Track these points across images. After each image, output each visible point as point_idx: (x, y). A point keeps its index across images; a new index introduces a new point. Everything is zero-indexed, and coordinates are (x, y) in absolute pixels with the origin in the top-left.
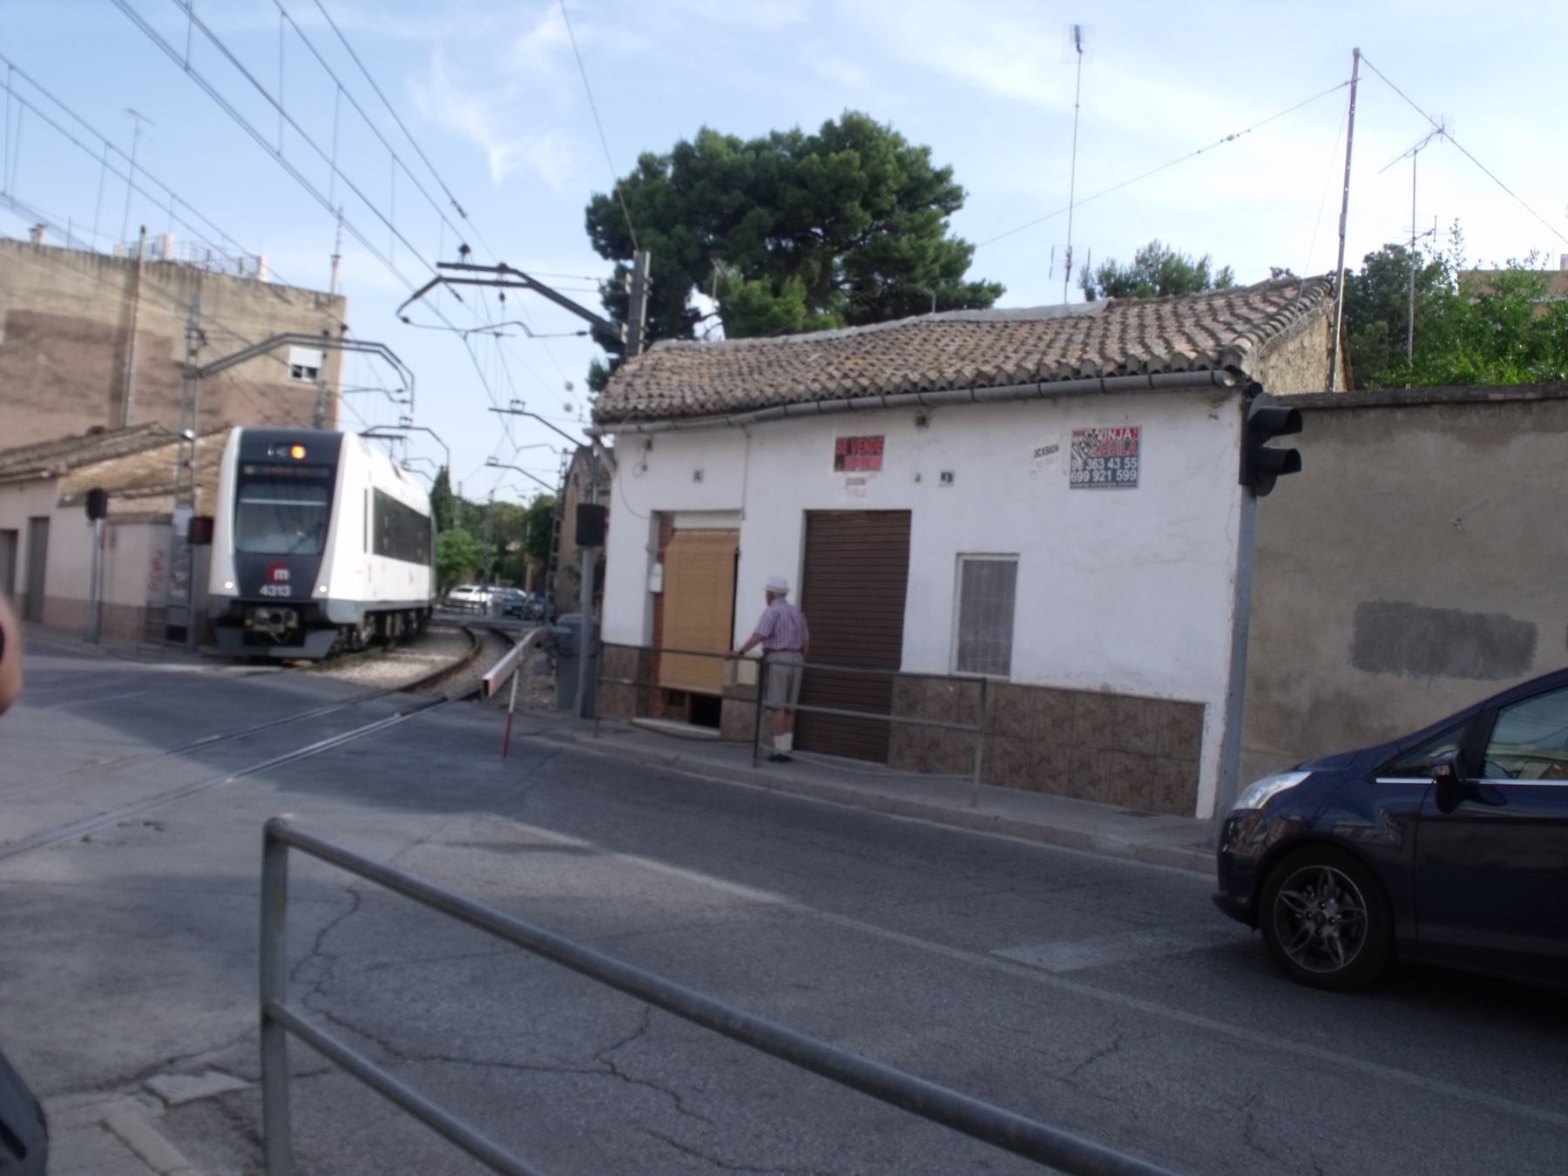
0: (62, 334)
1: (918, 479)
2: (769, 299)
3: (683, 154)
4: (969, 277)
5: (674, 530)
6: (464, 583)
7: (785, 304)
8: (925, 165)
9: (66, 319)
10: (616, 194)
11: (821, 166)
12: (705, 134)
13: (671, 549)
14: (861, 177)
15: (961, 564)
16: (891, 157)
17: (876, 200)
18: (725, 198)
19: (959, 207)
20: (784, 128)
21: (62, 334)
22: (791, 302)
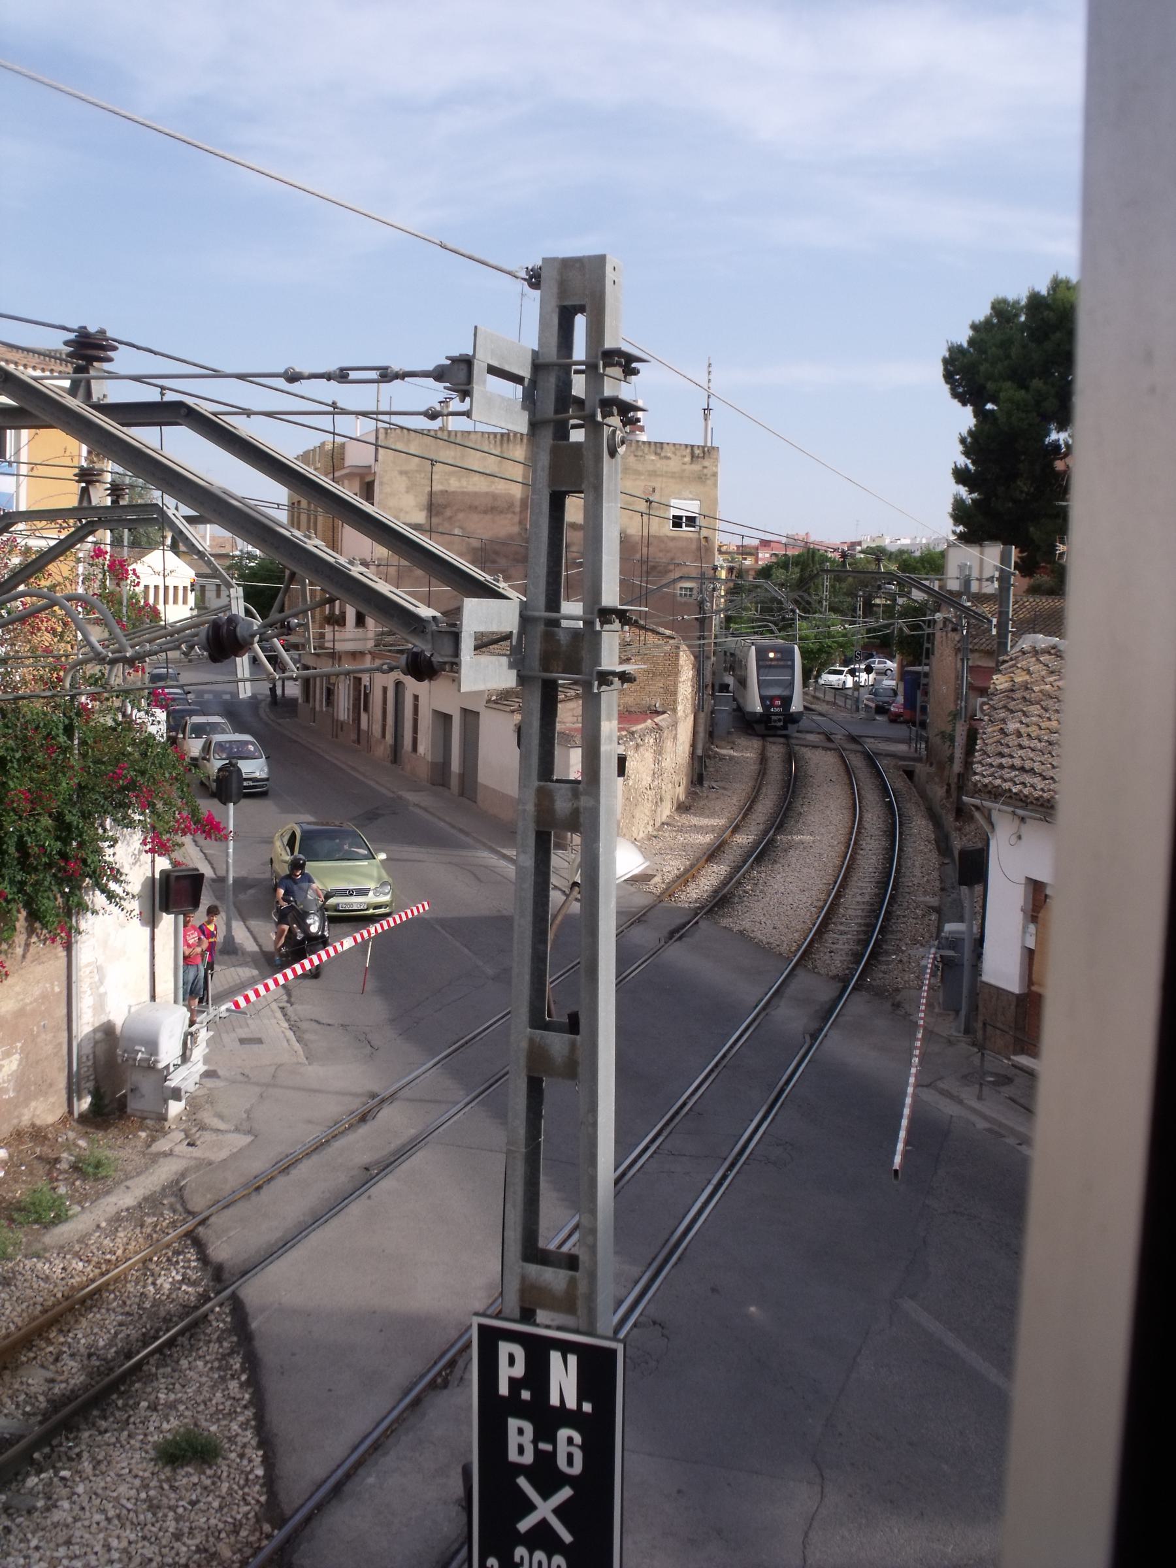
0: (473, 508)
9: (476, 493)
10: (971, 342)
21: (473, 508)
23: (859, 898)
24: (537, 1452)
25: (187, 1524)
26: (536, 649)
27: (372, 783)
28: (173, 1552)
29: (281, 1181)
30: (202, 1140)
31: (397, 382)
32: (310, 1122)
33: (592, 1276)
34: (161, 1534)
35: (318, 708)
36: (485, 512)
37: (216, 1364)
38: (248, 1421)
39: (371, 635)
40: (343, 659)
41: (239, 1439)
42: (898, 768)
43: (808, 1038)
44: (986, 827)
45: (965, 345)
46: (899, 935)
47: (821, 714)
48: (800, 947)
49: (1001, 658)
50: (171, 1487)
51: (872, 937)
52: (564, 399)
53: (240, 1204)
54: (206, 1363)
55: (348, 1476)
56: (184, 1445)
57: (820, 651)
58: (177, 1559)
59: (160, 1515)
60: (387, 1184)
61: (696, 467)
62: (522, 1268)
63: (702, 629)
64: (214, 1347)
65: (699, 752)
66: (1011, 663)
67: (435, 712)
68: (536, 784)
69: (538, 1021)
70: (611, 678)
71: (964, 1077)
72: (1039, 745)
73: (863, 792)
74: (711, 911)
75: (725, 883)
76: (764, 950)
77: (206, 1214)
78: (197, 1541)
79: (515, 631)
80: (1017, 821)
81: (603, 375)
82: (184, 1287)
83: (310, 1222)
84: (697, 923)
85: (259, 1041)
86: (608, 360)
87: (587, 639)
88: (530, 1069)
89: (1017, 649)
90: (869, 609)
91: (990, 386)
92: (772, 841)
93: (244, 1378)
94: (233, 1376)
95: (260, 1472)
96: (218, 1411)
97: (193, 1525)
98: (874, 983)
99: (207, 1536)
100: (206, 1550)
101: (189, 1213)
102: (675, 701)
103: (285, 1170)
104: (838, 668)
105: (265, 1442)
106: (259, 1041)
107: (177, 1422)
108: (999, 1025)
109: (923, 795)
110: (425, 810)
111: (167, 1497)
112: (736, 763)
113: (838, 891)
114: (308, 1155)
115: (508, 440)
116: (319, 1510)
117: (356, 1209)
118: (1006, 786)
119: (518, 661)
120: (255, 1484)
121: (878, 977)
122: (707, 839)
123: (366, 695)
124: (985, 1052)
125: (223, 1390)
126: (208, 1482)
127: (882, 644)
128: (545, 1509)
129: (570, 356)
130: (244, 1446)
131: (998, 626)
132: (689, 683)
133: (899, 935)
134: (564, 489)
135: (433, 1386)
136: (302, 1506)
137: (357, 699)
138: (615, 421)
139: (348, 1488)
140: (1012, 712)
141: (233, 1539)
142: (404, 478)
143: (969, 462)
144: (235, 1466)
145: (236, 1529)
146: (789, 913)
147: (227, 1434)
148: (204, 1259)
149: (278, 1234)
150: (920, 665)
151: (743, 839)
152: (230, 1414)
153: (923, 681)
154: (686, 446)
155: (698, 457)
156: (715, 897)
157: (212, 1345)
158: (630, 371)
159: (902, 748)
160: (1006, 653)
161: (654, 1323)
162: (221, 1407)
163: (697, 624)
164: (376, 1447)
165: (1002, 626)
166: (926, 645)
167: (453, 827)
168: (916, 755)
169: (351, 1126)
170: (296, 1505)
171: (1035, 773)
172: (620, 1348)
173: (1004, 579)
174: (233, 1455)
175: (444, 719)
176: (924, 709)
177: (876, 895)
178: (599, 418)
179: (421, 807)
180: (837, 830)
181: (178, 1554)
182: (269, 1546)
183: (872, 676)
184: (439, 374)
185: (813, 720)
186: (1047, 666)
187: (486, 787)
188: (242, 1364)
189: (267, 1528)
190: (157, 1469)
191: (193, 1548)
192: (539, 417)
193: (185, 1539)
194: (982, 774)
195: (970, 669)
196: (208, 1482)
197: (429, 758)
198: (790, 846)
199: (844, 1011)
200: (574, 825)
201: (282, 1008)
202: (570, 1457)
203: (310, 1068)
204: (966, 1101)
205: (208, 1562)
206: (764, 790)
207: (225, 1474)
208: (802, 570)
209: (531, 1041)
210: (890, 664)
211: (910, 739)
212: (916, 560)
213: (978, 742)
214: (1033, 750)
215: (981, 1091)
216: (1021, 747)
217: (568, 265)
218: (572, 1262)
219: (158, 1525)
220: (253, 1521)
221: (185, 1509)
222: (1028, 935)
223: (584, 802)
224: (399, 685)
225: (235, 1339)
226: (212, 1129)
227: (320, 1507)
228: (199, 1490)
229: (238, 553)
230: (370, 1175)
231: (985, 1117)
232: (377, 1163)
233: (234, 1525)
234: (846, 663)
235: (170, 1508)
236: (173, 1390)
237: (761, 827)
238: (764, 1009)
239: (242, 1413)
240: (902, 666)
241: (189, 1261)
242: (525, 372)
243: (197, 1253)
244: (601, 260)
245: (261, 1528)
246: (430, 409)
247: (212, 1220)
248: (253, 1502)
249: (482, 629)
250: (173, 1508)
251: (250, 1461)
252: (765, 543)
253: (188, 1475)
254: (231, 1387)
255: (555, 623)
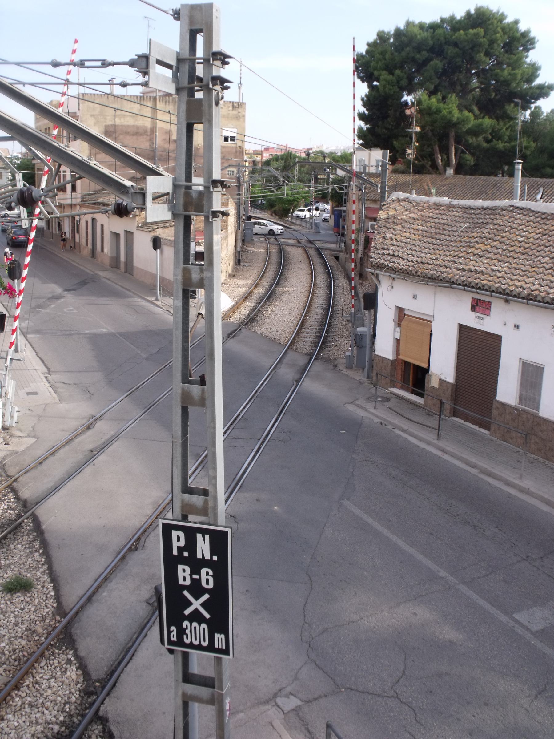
0: (127, 133)
1: (505, 325)
2: (441, 105)
3: (398, 33)
4: (538, 82)
5: (405, 315)
6: (300, 207)
7: (448, 109)
8: (517, 30)
9: (128, 126)
10: (367, 52)
11: (465, 36)
12: (408, 24)
13: (403, 323)
14: (484, 41)
15: (521, 362)
16: (499, 29)
17: (492, 51)
18: (418, 56)
19: (533, 48)
20: (446, 15)
21: (127, 133)
22: (451, 107)
23: (315, 317)
24: (192, 580)
25: (20, 619)
26: (181, 200)
27: (82, 267)
28: (15, 631)
29: (52, 459)
30: (12, 442)
31: (110, 67)
32: (63, 430)
33: (215, 498)
34: (8, 624)
35: (54, 232)
36: (133, 135)
37: (27, 546)
38: (45, 571)
39: (79, 196)
40: (66, 208)
41: (41, 579)
42: (331, 255)
43: (295, 382)
44: (375, 281)
45: (364, 53)
46: (335, 334)
47: (295, 230)
48: (289, 340)
49: (382, 203)
50: (11, 603)
51: (322, 335)
52: (193, 77)
53: (33, 471)
54: (23, 545)
55: (94, 593)
56: (15, 583)
57: (294, 200)
58: (17, 634)
59: (7, 615)
60: (102, 458)
61: (235, 112)
62: (182, 496)
63: (239, 190)
64: (26, 538)
65: (238, 249)
66: (387, 206)
67: (112, 232)
68: (182, 266)
69: (186, 379)
70: (218, 214)
71: (368, 398)
72: (401, 244)
73: (315, 267)
74: (247, 324)
75: (253, 311)
76: (272, 341)
77: (17, 476)
78: (26, 626)
79: (171, 192)
80: (391, 280)
81: (212, 64)
82: (9, 511)
83: (67, 478)
84: (240, 330)
85: (36, 393)
86: (215, 57)
87: (206, 195)
88: (182, 402)
89: (390, 199)
90: (316, 180)
91: (376, 73)
92: (274, 290)
93: (41, 551)
94: (36, 551)
95: (53, 593)
96: (30, 567)
97: (23, 619)
98: (324, 356)
99: (30, 623)
100: (30, 630)
101: (8, 476)
102: (227, 225)
103: (53, 454)
104: (302, 208)
105: (54, 580)
106: (36, 393)
107: (11, 573)
108: (383, 374)
109: (344, 268)
110: (109, 280)
111: (9, 607)
112: (256, 254)
113: (306, 313)
114: (63, 446)
115: (144, 99)
116: (82, 608)
117: (88, 470)
118: (386, 263)
119: (173, 208)
120: (51, 599)
121: (326, 353)
122: (243, 290)
123: (78, 225)
124: (378, 387)
125: (32, 558)
126: (28, 599)
127: (323, 197)
128: (197, 604)
129: (195, 55)
130: (44, 582)
131: (381, 188)
132: (233, 216)
133: (335, 334)
134: (193, 122)
135: (130, 550)
136: (74, 607)
137: (73, 227)
138: (218, 88)
139: (94, 598)
140: (388, 228)
141: (42, 624)
142: (93, 118)
143: (365, 110)
144: (40, 591)
145: (44, 619)
146: (283, 324)
147: (35, 577)
148: (17, 498)
149: (52, 484)
150: (341, 206)
151: (261, 290)
152: (36, 568)
153: (343, 214)
154: (230, 102)
155: (236, 107)
156: (248, 317)
157: (24, 537)
158: (225, 63)
159: (333, 246)
160: (385, 201)
161: (231, 516)
162: (31, 565)
163: (236, 188)
164: (106, 579)
165: (383, 188)
166: (344, 197)
167: (122, 287)
168: (340, 249)
169: (83, 431)
170: (71, 607)
171: (399, 257)
172: (229, 531)
173: (384, 166)
174: (39, 587)
175: (117, 235)
176: (343, 228)
177: (323, 315)
178: (211, 86)
179: (106, 278)
180: (304, 285)
181: (17, 632)
182: (60, 626)
183: (319, 212)
184: (132, 64)
185: (291, 233)
186: (404, 207)
187: (138, 268)
188: (40, 545)
189: (58, 618)
190: (3, 595)
191: (24, 629)
192: (180, 85)
193: (20, 625)
194: (375, 257)
195: (366, 208)
196: (28, 599)
197: (110, 255)
198: (283, 293)
199: (311, 369)
200: (201, 285)
201: (46, 377)
202: (208, 581)
203: (61, 405)
204: (369, 410)
205: (32, 635)
206: (269, 266)
207: (36, 595)
208: (285, 162)
209: (183, 389)
210: (328, 207)
211: (337, 242)
212: (338, 157)
213: (373, 243)
214: (398, 247)
215: (376, 405)
216: (393, 245)
217: (193, 8)
218: (205, 493)
219: (6, 620)
220: (51, 615)
221: (19, 612)
222: (396, 333)
223: (206, 274)
224: (93, 220)
225: (35, 534)
226: (16, 436)
227: (82, 607)
228: (24, 603)
229: (10, 156)
230: (94, 454)
231: (378, 417)
232: (97, 448)
233: (42, 617)
234: (306, 206)
235: (11, 612)
236: (8, 559)
237: (269, 284)
238: (274, 369)
239: (42, 567)
240: (333, 208)
241: (10, 499)
242: (173, 63)
243: (14, 495)
244: (210, 6)
245: (55, 618)
246: (122, 82)
247: (20, 479)
248: (50, 607)
249: (156, 191)
250: (13, 612)
251: (47, 589)
252: (267, 149)
253: (18, 597)
254: (35, 556)
255: (189, 188)
